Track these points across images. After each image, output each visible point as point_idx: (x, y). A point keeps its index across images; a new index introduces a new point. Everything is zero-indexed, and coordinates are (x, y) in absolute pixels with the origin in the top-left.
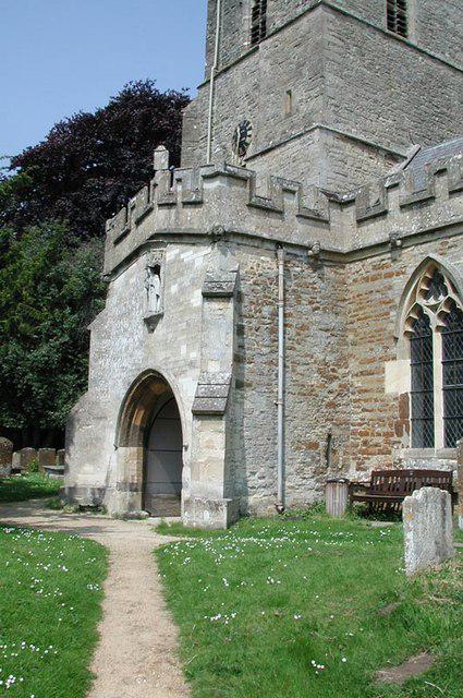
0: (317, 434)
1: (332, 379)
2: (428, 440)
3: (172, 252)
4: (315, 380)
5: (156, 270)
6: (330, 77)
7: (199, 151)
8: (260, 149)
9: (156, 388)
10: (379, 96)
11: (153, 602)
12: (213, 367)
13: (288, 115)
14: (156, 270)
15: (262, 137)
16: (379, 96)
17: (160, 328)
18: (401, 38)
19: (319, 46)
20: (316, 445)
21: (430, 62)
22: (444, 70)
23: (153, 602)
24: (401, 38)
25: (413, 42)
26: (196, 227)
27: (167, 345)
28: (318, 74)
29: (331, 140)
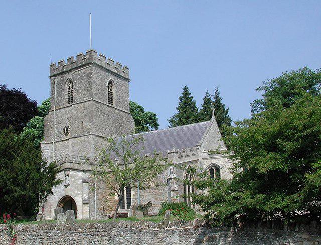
0: (101, 207)
1: (104, 197)
2: (123, 208)
3: (71, 172)
4: (101, 197)
5: (68, 175)
6: (94, 120)
7: (50, 131)
8: (73, 136)
9: (67, 199)
10: (106, 123)
11: (227, 160)
12: (85, 195)
13: (82, 128)
14: (68, 175)
15: (73, 132)
16: (106, 123)
17: (69, 187)
18: (111, 105)
19: (91, 112)
20: (101, 209)
21: (119, 111)
22: (123, 113)
23: (227, 160)
24: (111, 105)
25: (114, 106)
26: (79, 168)
27: (71, 191)
28: (91, 119)
29: (95, 137)
